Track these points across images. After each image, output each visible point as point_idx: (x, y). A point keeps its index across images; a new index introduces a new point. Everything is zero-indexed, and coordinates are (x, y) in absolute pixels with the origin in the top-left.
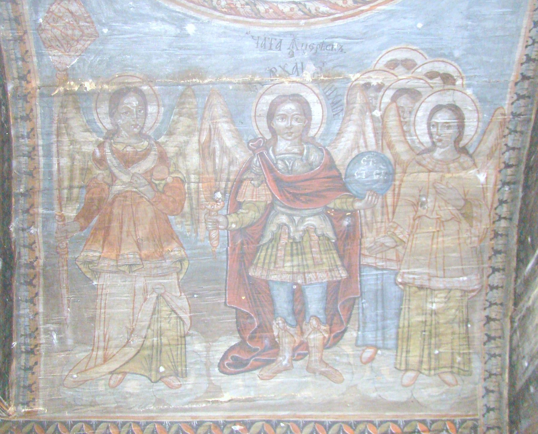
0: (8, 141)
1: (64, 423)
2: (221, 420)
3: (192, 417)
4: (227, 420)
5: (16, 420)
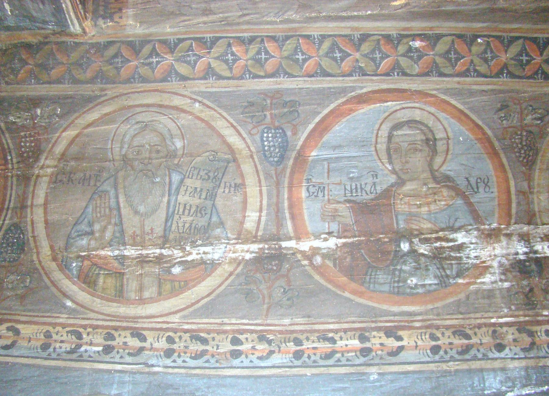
0: (18, 241)
1: (164, 42)
2: (394, 33)
3: (352, 29)
4: (402, 33)
5: (94, 41)
